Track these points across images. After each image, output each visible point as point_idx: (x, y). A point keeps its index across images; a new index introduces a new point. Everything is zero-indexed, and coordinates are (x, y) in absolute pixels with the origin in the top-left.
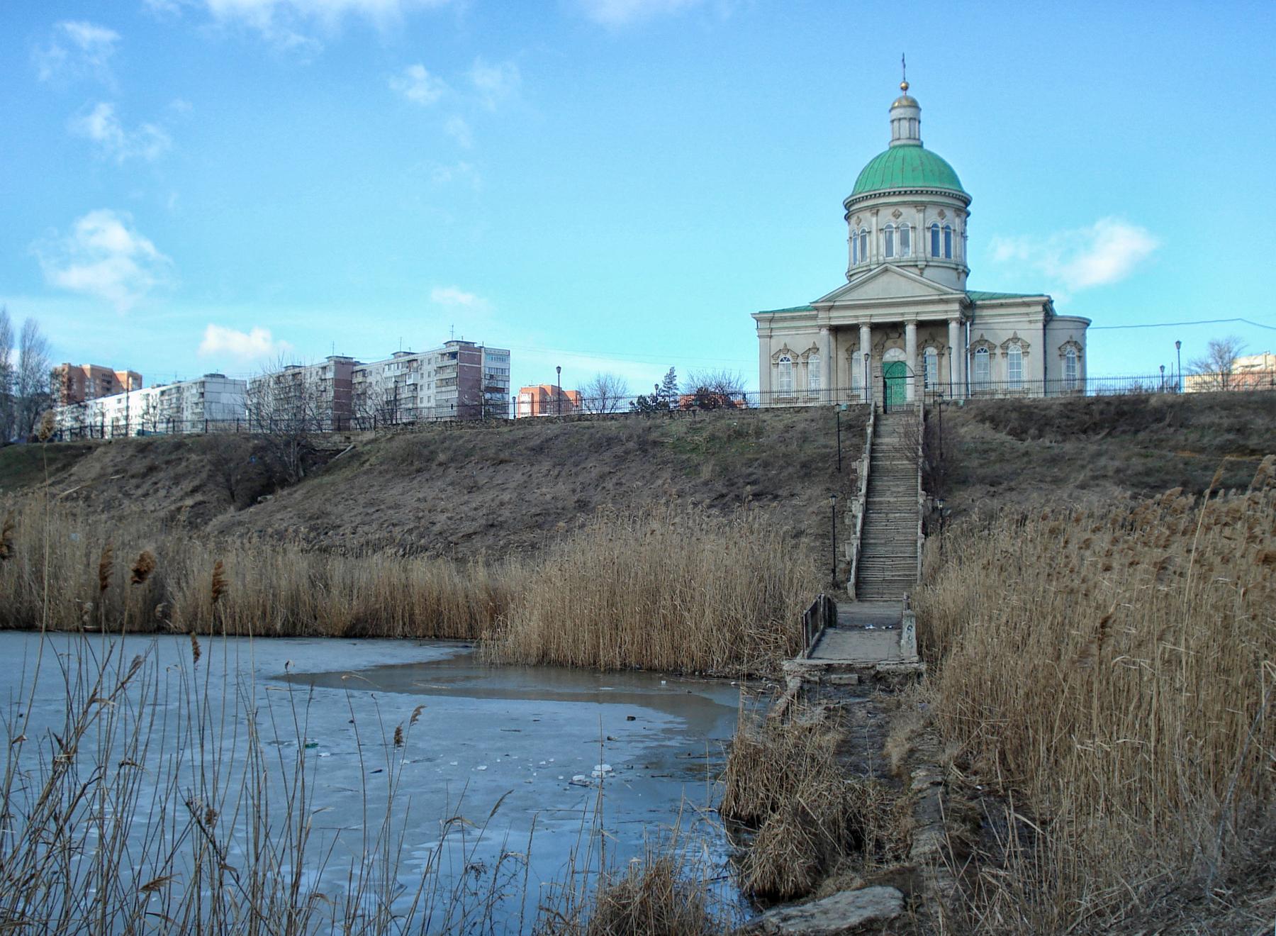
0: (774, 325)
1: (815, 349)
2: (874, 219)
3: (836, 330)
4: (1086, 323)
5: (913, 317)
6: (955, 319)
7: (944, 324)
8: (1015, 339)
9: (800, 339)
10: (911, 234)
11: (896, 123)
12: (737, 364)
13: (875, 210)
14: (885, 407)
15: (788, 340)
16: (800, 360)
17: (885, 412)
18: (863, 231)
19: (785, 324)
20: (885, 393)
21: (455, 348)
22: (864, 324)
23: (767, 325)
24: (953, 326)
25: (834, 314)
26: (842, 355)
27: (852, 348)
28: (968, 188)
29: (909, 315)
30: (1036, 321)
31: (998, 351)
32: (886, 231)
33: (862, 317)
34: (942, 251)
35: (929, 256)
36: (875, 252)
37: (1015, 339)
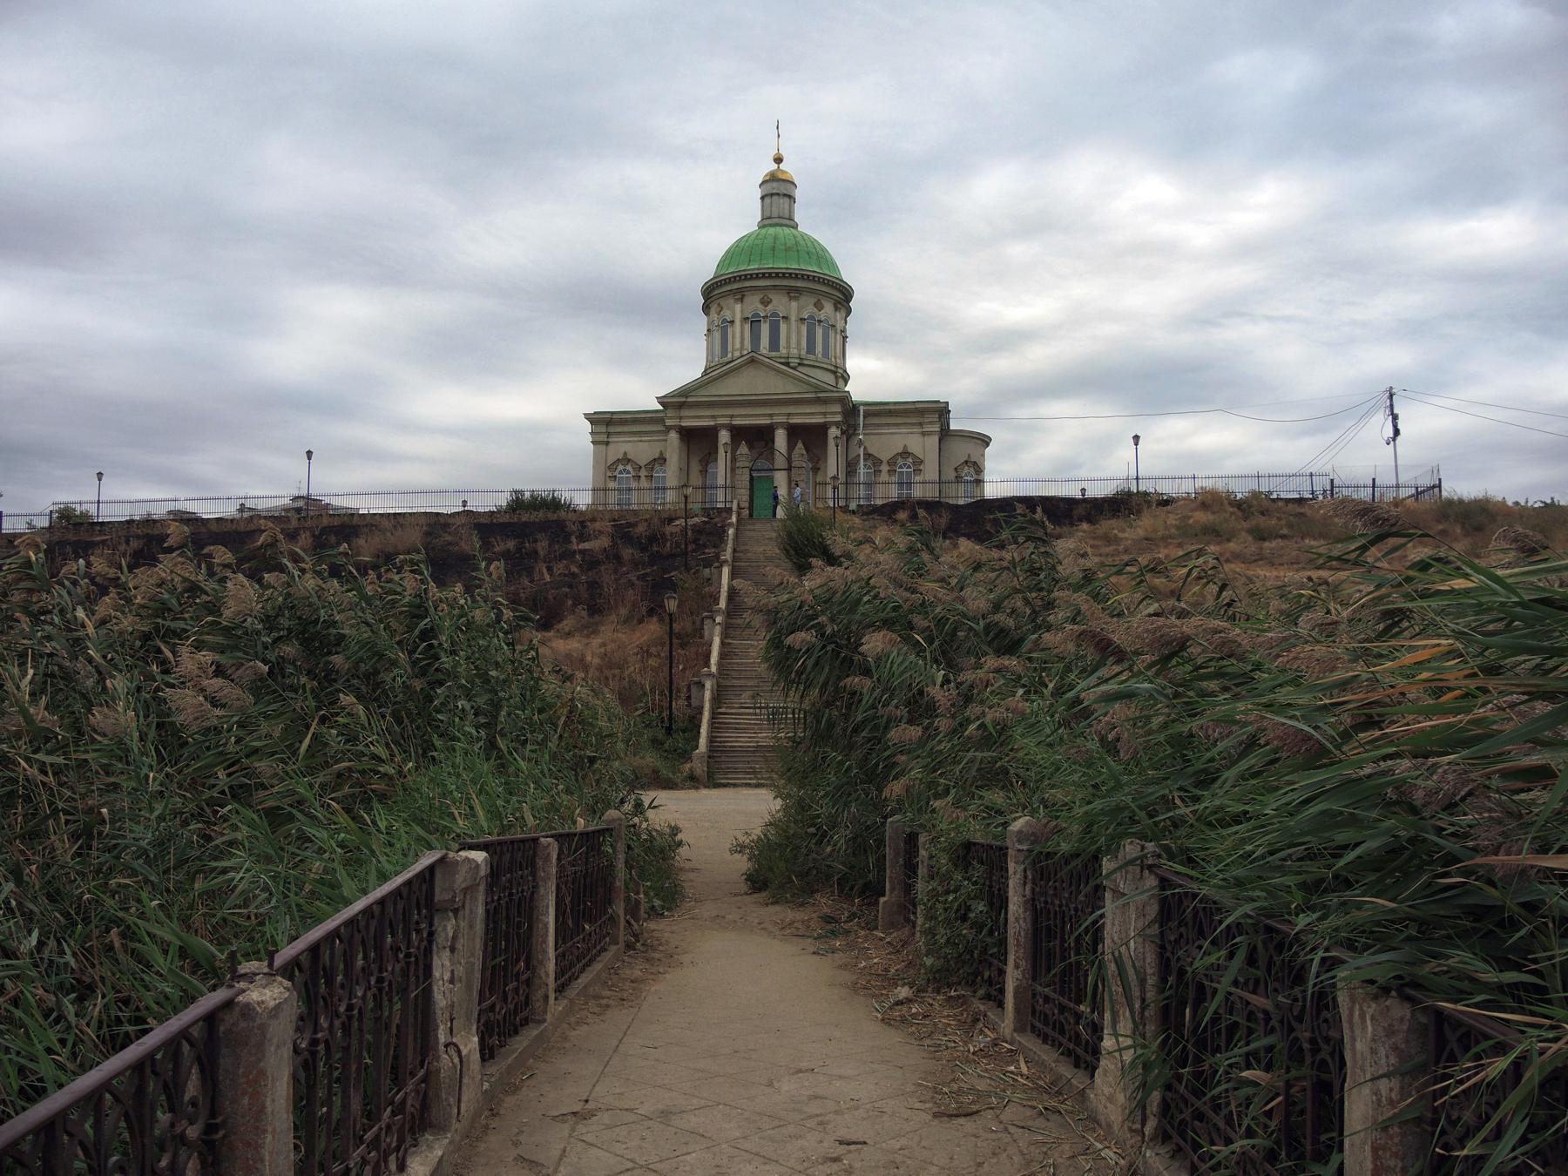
0: (612, 429)
1: (661, 460)
2: (738, 307)
3: (688, 435)
4: (985, 441)
5: (782, 419)
6: (837, 424)
7: (822, 429)
8: (905, 454)
9: (643, 450)
10: (783, 327)
11: (767, 200)
12: (570, 473)
13: (740, 295)
14: (751, 508)
15: (627, 448)
16: (643, 473)
17: (751, 515)
18: (725, 321)
19: (626, 429)
20: (751, 489)
21: (301, 503)
22: (723, 426)
23: (603, 429)
24: (834, 432)
25: (685, 413)
26: (695, 467)
27: (709, 457)
28: (848, 276)
29: (780, 416)
30: (930, 433)
31: (885, 468)
32: (754, 322)
33: (722, 417)
34: (819, 348)
35: (803, 352)
36: (738, 345)
37: (905, 454)
